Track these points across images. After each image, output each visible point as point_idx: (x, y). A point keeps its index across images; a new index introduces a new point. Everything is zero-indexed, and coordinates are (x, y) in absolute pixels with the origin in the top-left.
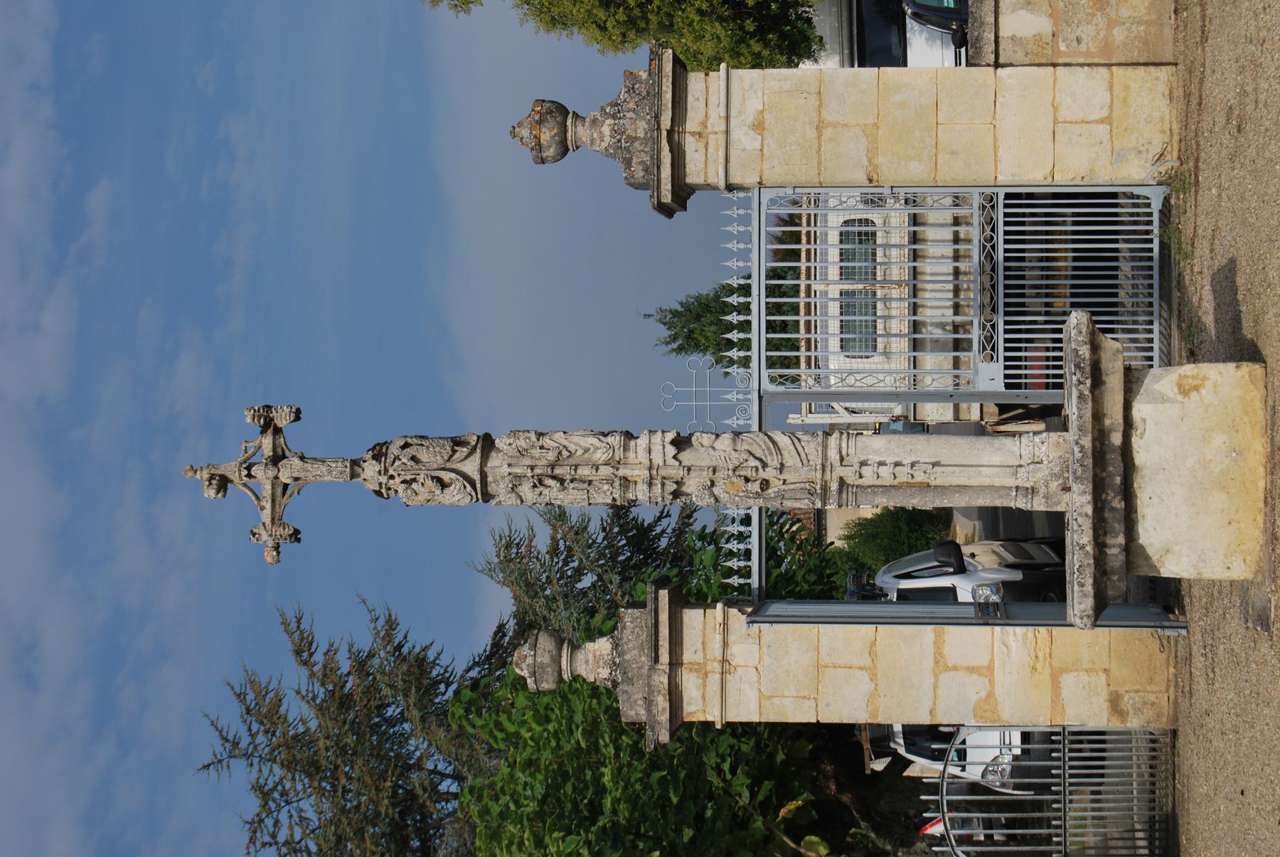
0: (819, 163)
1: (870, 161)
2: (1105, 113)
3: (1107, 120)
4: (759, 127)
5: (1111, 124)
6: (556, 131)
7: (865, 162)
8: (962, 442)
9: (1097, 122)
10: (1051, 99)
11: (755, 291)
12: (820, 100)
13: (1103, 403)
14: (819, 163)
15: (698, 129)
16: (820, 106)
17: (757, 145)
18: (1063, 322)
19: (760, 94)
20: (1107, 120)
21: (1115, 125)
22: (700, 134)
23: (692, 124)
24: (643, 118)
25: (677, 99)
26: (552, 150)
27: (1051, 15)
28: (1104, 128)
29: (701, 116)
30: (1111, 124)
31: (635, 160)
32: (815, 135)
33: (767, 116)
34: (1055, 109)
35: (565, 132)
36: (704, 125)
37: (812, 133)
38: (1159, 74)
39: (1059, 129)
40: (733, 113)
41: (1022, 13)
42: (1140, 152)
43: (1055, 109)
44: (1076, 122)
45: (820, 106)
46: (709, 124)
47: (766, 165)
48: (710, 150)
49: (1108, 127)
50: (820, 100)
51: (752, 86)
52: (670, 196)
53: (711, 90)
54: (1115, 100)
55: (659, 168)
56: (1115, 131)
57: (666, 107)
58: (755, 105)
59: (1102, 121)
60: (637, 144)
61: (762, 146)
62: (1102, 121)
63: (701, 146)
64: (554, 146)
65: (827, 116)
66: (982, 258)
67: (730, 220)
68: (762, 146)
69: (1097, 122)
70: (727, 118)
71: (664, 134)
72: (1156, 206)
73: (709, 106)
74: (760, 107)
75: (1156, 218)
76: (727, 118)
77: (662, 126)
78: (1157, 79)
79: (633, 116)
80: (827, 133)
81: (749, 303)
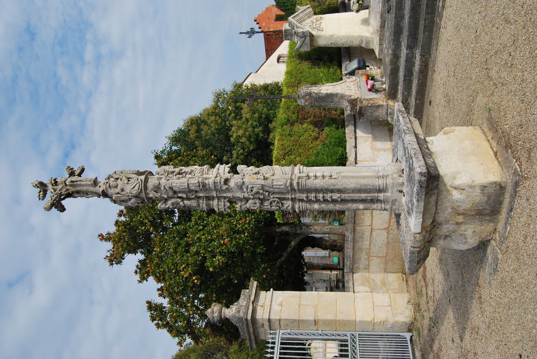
0: (299, 314)
1: (315, 314)
2: (389, 304)
3: (390, 306)
4: (281, 305)
5: (391, 306)
6: (219, 308)
7: (313, 314)
8: (378, 20)
9: (387, 306)
10: (372, 300)
11: (277, 343)
12: (300, 299)
13: (429, 92)
14: (299, 314)
15: (262, 305)
16: (300, 300)
17: (280, 309)
18: (406, 103)
19: (282, 297)
20: (390, 306)
21: (392, 307)
22: (262, 306)
23: (260, 303)
24: (245, 301)
25: (257, 295)
26: (216, 314)
27: (369, 287)
28: (389, 308)
29: (263, 302)
30: (391, 306)
31: (241, 311)
32: (298, 307)
33: (283, 302)
34: (373, 303)
35: (222, 310)
36: (264, 304)
37: (297, 307)
38: (405, 295)
39: (375, 308)
40: (273, 301)
41: (361, 286)
42: (402, 314)
43: (373, 303)
44: (380, 306)
45: (300, 300)
46: (265, 304)
47: (282, 314)
48: (265, 310)
49: (391, 307)
50: (300, 299)
51: (279, 295)
52: (250, 317)
53: (267, 296)
54: (392, 301)
55: (248, 309)
56: (393, 309)
57: (253, 295)
58: (280, 299)
59: (388, 306)
60: (242, 307)
61: (281, 309)
62: (388, 306)
63: (262, 309)
64: (217, 312)
65: (302, 302)
66: (352, 351)
67: (268, 348)
68: (281, 309)
69: (387, 306)
70: (271, 302)
71: (251, 301)
72: (408, 339)
73: (266, 299)
74: (282, 300)
75: (409, 342)
76: (271, 302)
77: (251, 299)
78: (404, 296)
79: (243, 300)
80: (302, 307)
81: (275, 347)
